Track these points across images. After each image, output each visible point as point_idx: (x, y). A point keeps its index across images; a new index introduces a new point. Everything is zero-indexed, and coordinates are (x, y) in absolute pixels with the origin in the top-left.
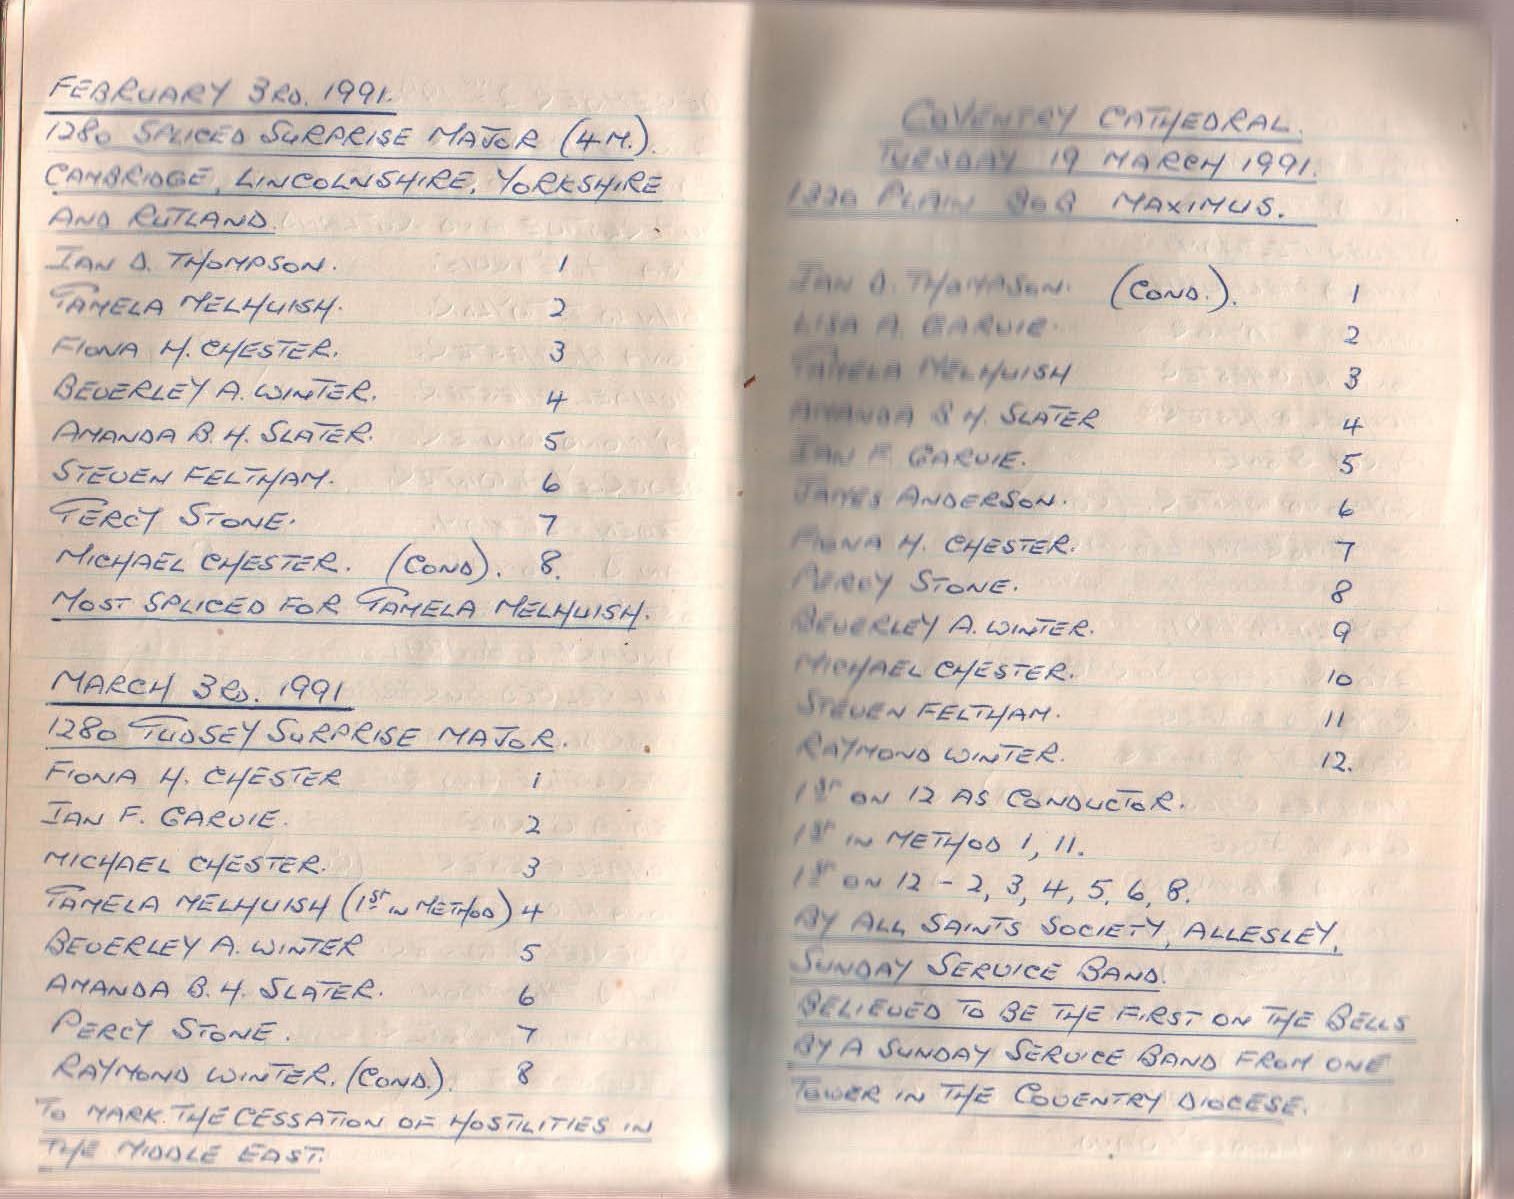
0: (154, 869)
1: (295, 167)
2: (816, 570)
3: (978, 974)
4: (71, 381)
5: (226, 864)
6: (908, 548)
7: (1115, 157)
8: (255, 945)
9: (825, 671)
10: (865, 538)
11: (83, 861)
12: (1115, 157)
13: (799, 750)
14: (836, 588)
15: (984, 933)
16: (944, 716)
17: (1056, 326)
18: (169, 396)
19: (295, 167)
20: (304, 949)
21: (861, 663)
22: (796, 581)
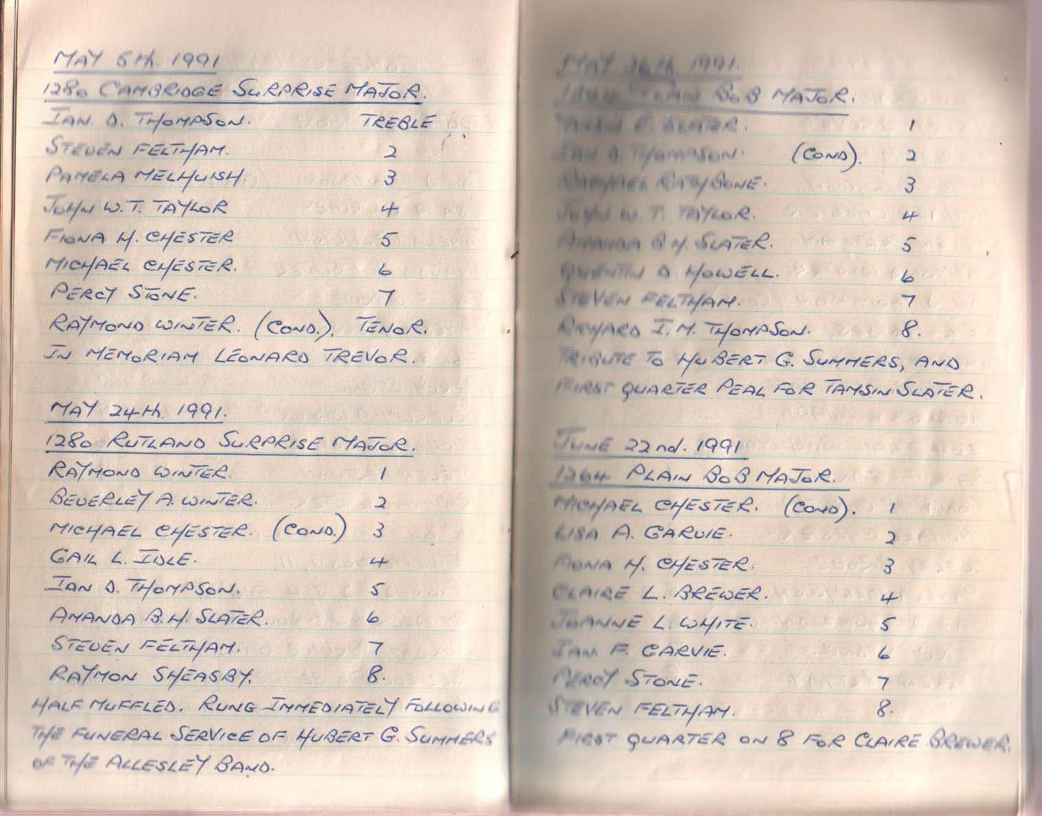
0: (628, 509)
1: (203, 111)
2: (570, 672)
3: (683, 535)
4: (334, 733)
5: (174, 237)
6: (631, 568)
7: (781, 93)
8: (184, 500)
9: (572, 509)
10: (602, 562)
11: (111, 676)
12: (781, 93)
13: (657, 185)
14: (581, 391)
15: (687, 480)
16: (654, 712)
17: (743, 153)
18: (178, 563)
19: (203, 111)
20: (217, 501)
21: (599, 503)
22: (555, 679)
